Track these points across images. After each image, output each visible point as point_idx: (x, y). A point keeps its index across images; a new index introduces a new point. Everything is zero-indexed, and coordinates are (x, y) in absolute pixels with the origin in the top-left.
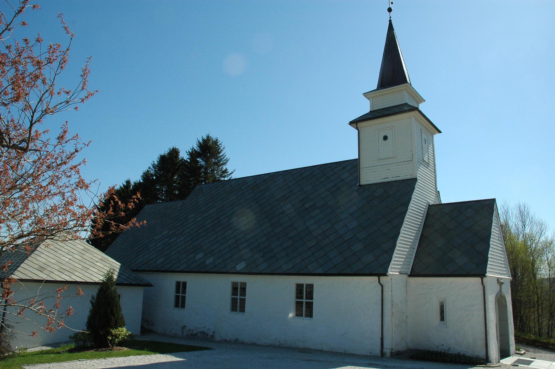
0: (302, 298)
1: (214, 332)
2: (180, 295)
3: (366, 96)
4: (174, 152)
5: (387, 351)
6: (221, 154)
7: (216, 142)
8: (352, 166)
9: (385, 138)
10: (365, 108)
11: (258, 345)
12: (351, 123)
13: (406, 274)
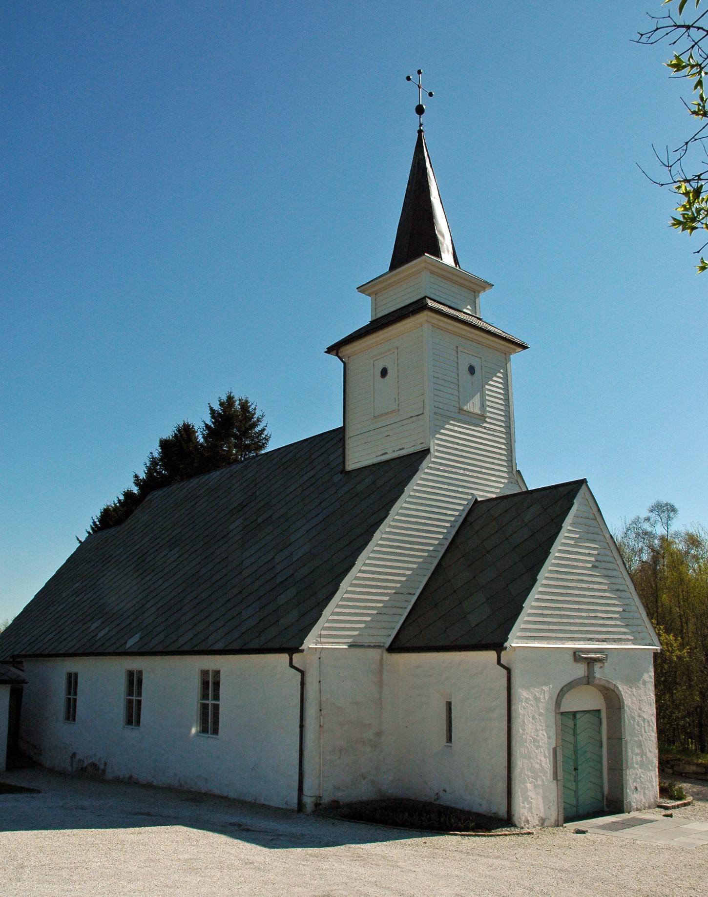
0: (208, 699)
1: (106, 764)
2: (210, 702)
3: (363, 292)
4: (186, 431)
5: (308, 801)
6: (258, 429)
7: (245, 406)
8: (335, 439)
9: (384, 373)
11: (156, 788)
12: (330, 350)
13: (378, 647)
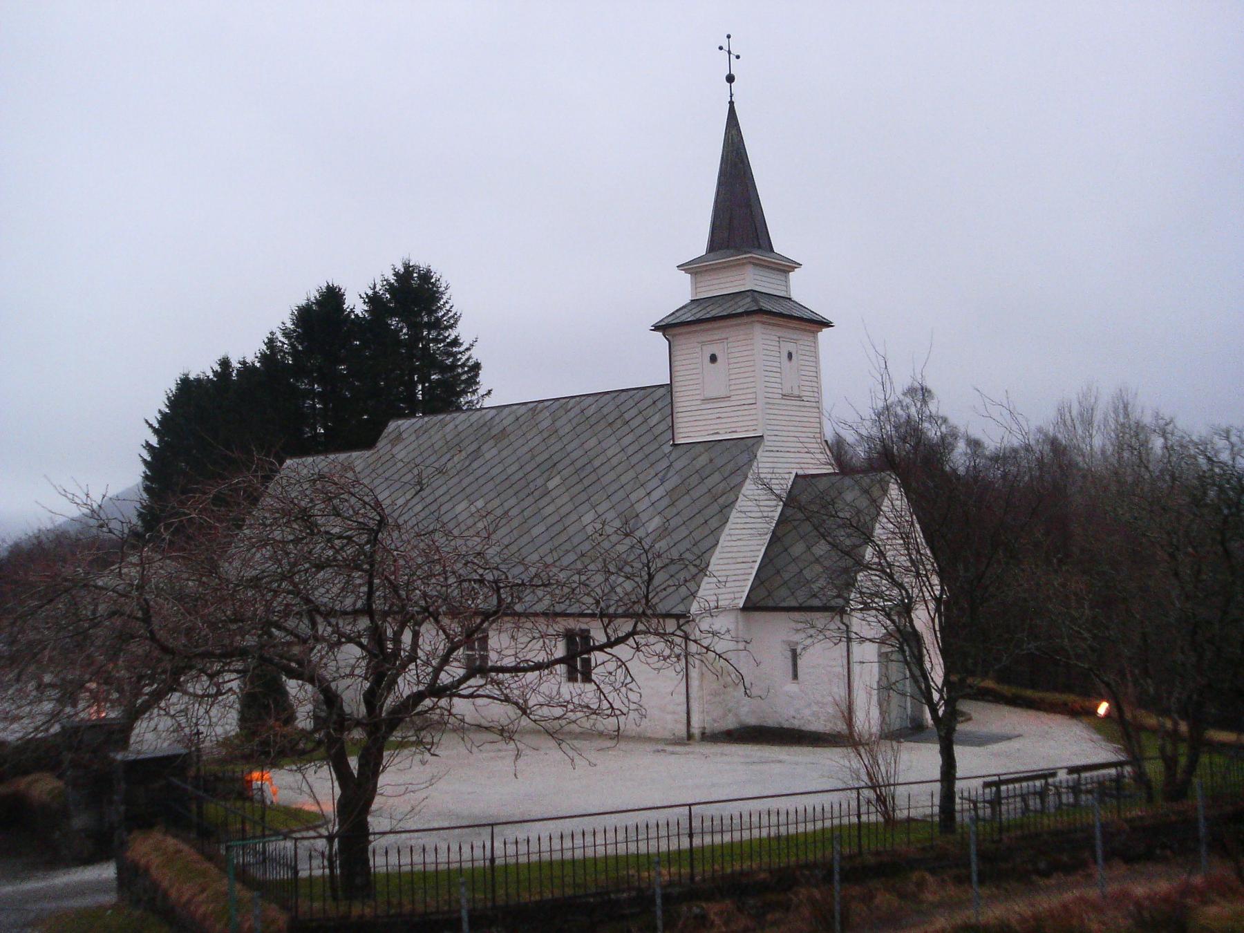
4: (332, 297)
5: (696, 730)
7: (426, 276)
10: (678, 293)
12: (657, 328)
